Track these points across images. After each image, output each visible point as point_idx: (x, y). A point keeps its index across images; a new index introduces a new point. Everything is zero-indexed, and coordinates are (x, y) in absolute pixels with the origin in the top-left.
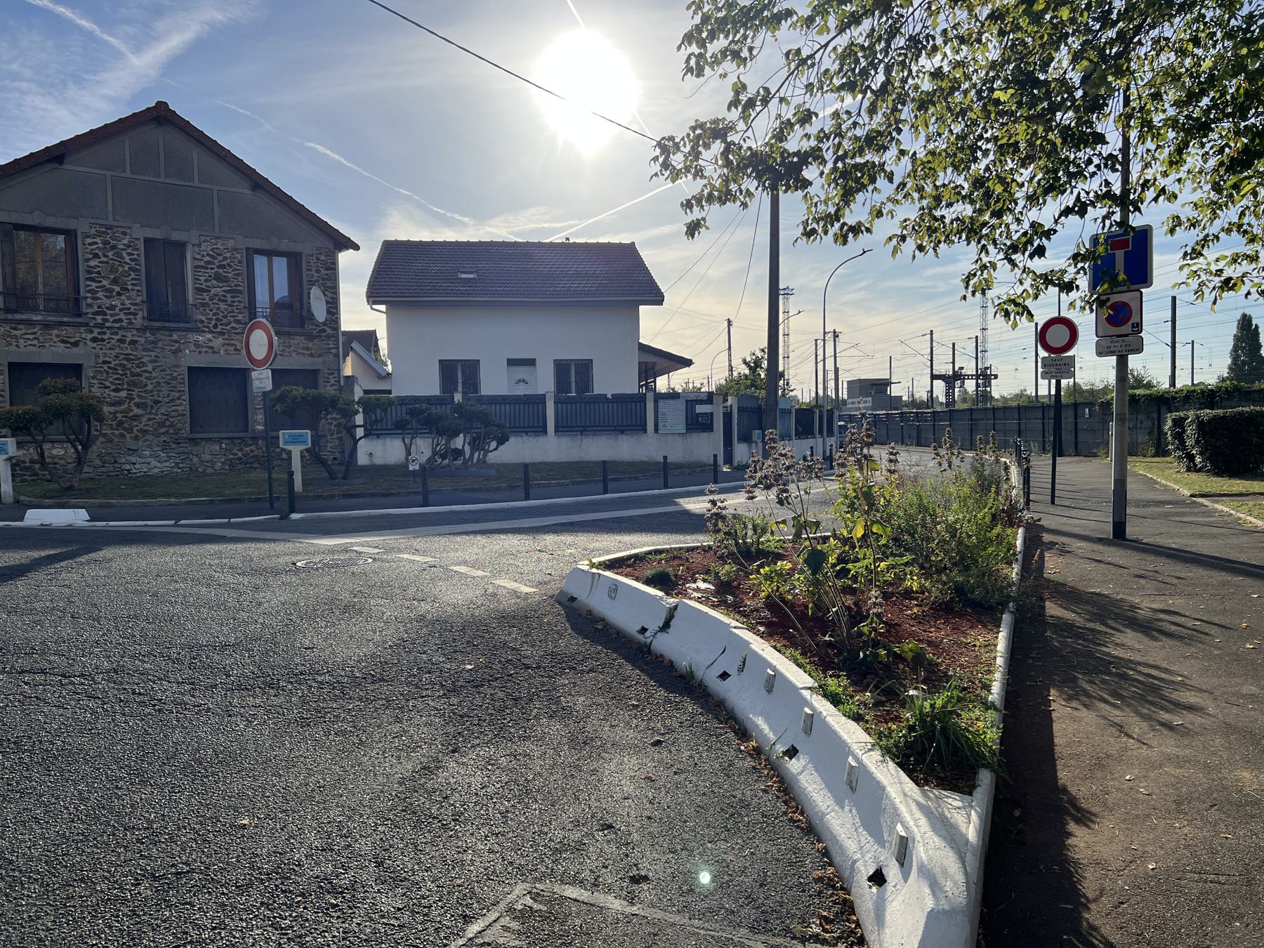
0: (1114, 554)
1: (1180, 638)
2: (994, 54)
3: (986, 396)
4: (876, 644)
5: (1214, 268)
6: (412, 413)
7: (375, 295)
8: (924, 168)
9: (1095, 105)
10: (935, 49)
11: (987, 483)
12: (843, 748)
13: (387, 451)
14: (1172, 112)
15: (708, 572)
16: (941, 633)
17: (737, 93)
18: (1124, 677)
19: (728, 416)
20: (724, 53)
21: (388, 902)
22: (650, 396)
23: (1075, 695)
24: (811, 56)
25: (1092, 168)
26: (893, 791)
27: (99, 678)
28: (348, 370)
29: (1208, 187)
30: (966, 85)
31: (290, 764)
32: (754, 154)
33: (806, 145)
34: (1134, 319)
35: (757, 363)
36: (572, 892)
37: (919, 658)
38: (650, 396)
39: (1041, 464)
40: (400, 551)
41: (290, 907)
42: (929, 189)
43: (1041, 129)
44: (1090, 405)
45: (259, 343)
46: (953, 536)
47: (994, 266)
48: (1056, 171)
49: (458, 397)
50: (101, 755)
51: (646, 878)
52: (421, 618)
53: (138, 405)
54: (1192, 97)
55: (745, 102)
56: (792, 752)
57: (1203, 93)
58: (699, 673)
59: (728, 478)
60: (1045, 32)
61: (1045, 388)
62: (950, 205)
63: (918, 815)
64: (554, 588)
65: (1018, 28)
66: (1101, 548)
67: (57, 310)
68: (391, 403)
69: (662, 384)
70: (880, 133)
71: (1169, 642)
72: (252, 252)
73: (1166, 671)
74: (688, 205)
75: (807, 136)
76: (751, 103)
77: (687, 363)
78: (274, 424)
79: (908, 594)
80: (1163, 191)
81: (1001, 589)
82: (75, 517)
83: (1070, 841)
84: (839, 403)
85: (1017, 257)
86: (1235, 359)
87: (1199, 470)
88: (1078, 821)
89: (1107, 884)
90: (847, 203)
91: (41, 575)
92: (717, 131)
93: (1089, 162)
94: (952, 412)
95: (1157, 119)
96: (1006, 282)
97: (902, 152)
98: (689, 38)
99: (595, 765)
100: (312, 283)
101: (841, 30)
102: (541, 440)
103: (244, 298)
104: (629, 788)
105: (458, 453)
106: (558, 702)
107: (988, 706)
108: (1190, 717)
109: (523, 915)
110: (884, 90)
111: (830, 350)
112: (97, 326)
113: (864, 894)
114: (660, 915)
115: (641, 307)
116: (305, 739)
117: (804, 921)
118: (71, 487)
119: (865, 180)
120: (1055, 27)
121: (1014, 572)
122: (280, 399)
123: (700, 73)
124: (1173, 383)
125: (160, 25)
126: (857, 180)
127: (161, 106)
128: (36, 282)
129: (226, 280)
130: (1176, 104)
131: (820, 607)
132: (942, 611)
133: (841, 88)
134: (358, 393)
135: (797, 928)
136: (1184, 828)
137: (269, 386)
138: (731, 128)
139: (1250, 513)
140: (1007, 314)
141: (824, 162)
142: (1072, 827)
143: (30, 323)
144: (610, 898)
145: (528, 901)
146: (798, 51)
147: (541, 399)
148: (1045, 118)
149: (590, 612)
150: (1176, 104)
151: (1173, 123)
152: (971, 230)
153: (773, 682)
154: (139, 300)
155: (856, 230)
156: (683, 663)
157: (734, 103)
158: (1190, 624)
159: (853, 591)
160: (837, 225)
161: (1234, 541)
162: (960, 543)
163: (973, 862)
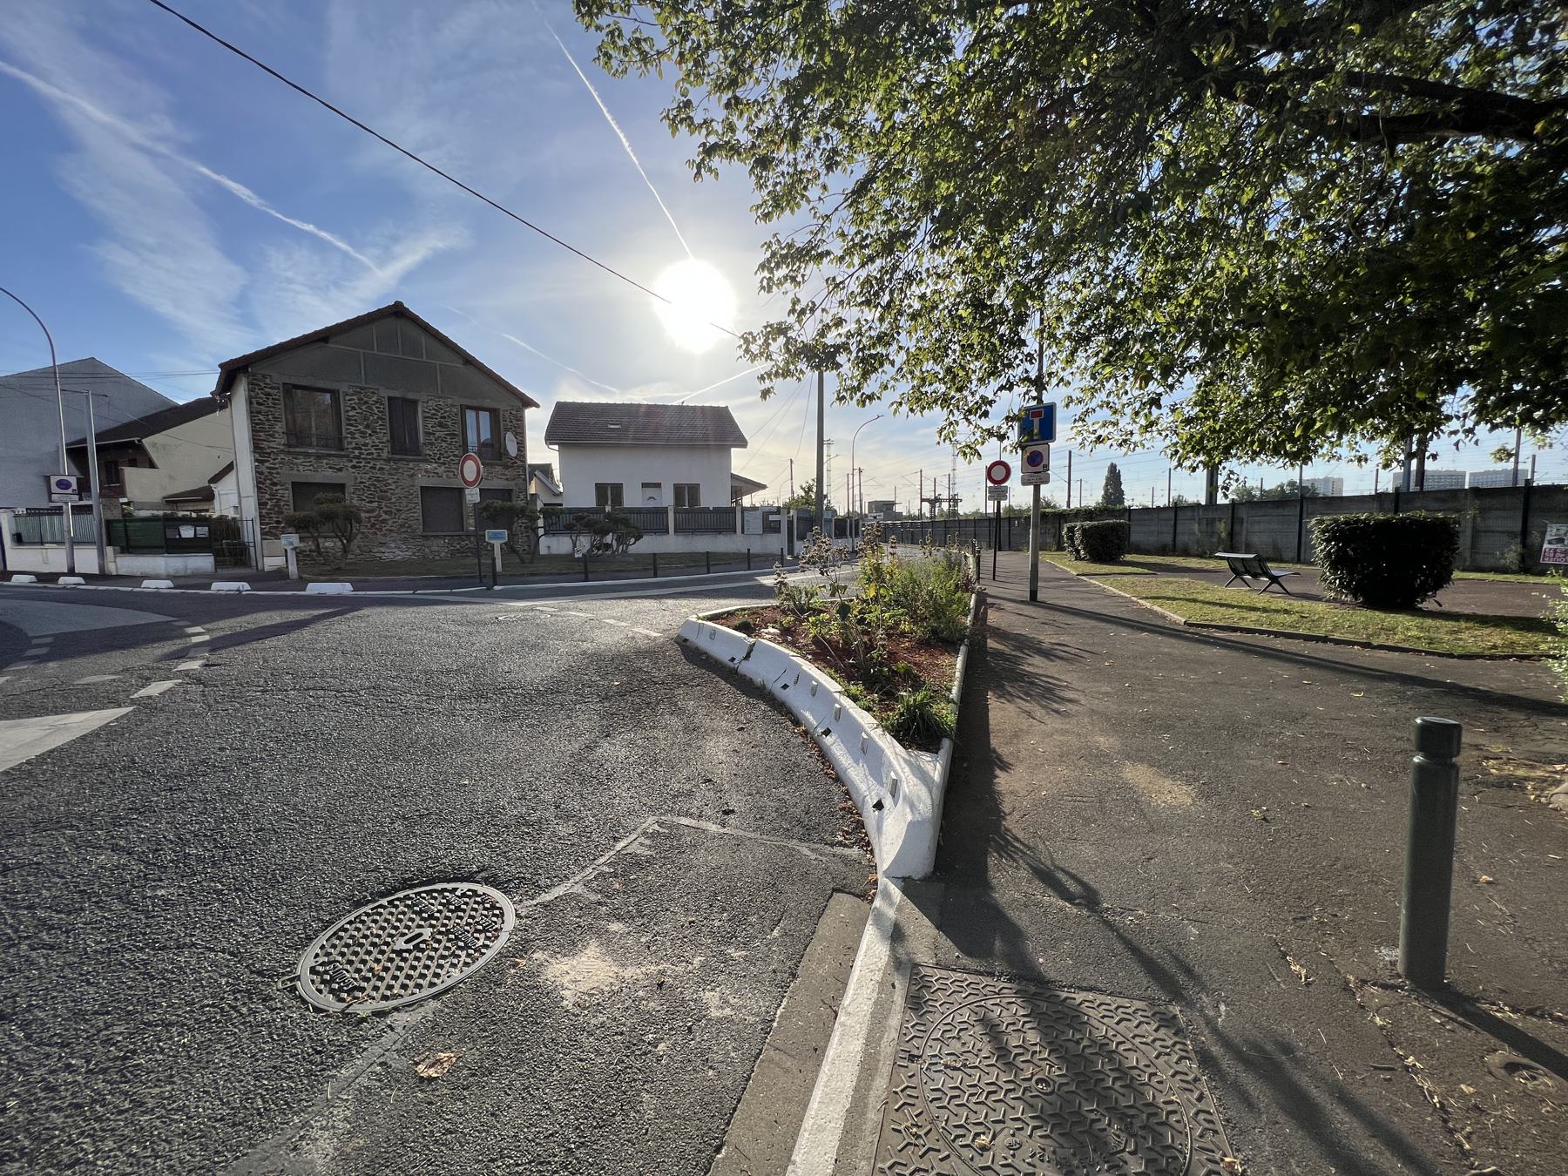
0: (1029, 610)
1: (1066, 660)
2: (960, 288)
3: (955, 513)
4: (881, 664)
5: (1091, 430)
6: (579, 519)
7: (551, 437)
8: (915, 359)
9: (1021, 320)
10: (921, 280)
11: (953, 565)
12: (858, 728)
13: (555, 545)
14: (1068, 328)
15: (775, 622)
16: (923, 658)
17: (794, 304)
18: (1032, 683)
19: (790, 523)
20: (786, 277)
21: (563, 830)
22: (739, 509)
23: (1003, 694)
24: (842, 282)
25: (1018, 361)
26: (889, 752)
27: (362, 693)
28: (532, 489)
29: (1088, 378)
30: (941, 307)
31: (496, 746)
32: (805, 346)
33: (839, 341)
34: (1044, 462)
35: (810, 489)
36: (684, 821)
37: (908, 672)
38: (739, 509)
39: (987, 556)
40: (569, 610)
41: (497, 835)
42: (918, 373)
43: (987, 336)
44: (1019, 518)
45: (470, 469)
46: (931, 597)
47: (957, 423)
48: (996, 363)
49: (608, 509)
50: (365, 742)
51: (733, 811)
52: (584, 652)
53: (386, 512)
54: (1080, 319)
55: (800, 312)
56: (827, 732)
57: (1087, 317)
58: (769, 686)
59: (791, 563)
60: (990, 272)
61: (991, 508)
62: (931, 384)
63: (904, 765)
64: (674, 633)
65: (974, 270)
66: (1022, 606)
67: (326, 446)
68: (562, 511)
69: (747, 501)
70: (886, 334)
71: (1059, 662)
72: (464, 408)
73: (1058, 679)
74: (762, 378)
75: (840, 335)
76: (803, 312)
77: (763, 487)
78: (482, 524)
79: (903, 634)
80: (1062, 380)
81: (960, 631)
82: (344, 588)
83: (996, 780)
84: (863, 517)
85: (971, 418)
86: (1106, 491)
87: (1083, 559)
88: (1002, 769)
89: (1017, 805)
90: (865, 380)
91: (319, 626)
92: (781, 330)
93: (1016, 357)
94: (933, 522)
95: (1059, 333)
96: (964, 432)
97: (901, 348)
98: (762, 267)
99: (700, 743)
100: (507, 430)
101: (863, 265)
102: (664, 538)
103: (459, 439)
104: (722, 757)
105: (608, 546)
106: (676, 705)
107: (949, 701)
108: (1070, 706)
109: (654, 836)
110: (888, 306)
111: (856, 482)
112: (355, 457)
113: (870, 816)
114: (741, 833)
115: (733, 450)
116: (505, 731)
117: (833, 834)
118: (339, 569)
119: (877, 365)
120: (997, 270)
121: (968, 621)
122: (485, 509)
123: (769, 290)
124: (1068, 505)
125: (397, 249)
126: (872, 365)
127: (398, 305)
128: (310, 428)
129: (446, 427)
130: (1071, 324)
131: (847, 642)
132: (924, 644)
133: (862, 303)
134: (540, 505)
135: (828, 837)
136: (1064, 771)
137: (478, 499)
138: (790, 328)
139: (1111, 585)
140: (965, 454)
141: (850, 352)
142: (998, 772)
143: (308, 455)
144: (710, 824)
145: (656, 827)
146: (834, 279)
147: (664, 511)
148: (991, 329)
149: (697, 649)
150: (1071, 324)
151: (1068, 336)
152: (945, 401)
153: (816, 690)
154: (385, 439)
155: (871, 397)
156: (758, 680)
157: (793, 311)
158: (1073, 651)
159: (868, 633)
160: (859, 394)
161: (1101, 602)
162: (935, 602)
163: (937, 793)
